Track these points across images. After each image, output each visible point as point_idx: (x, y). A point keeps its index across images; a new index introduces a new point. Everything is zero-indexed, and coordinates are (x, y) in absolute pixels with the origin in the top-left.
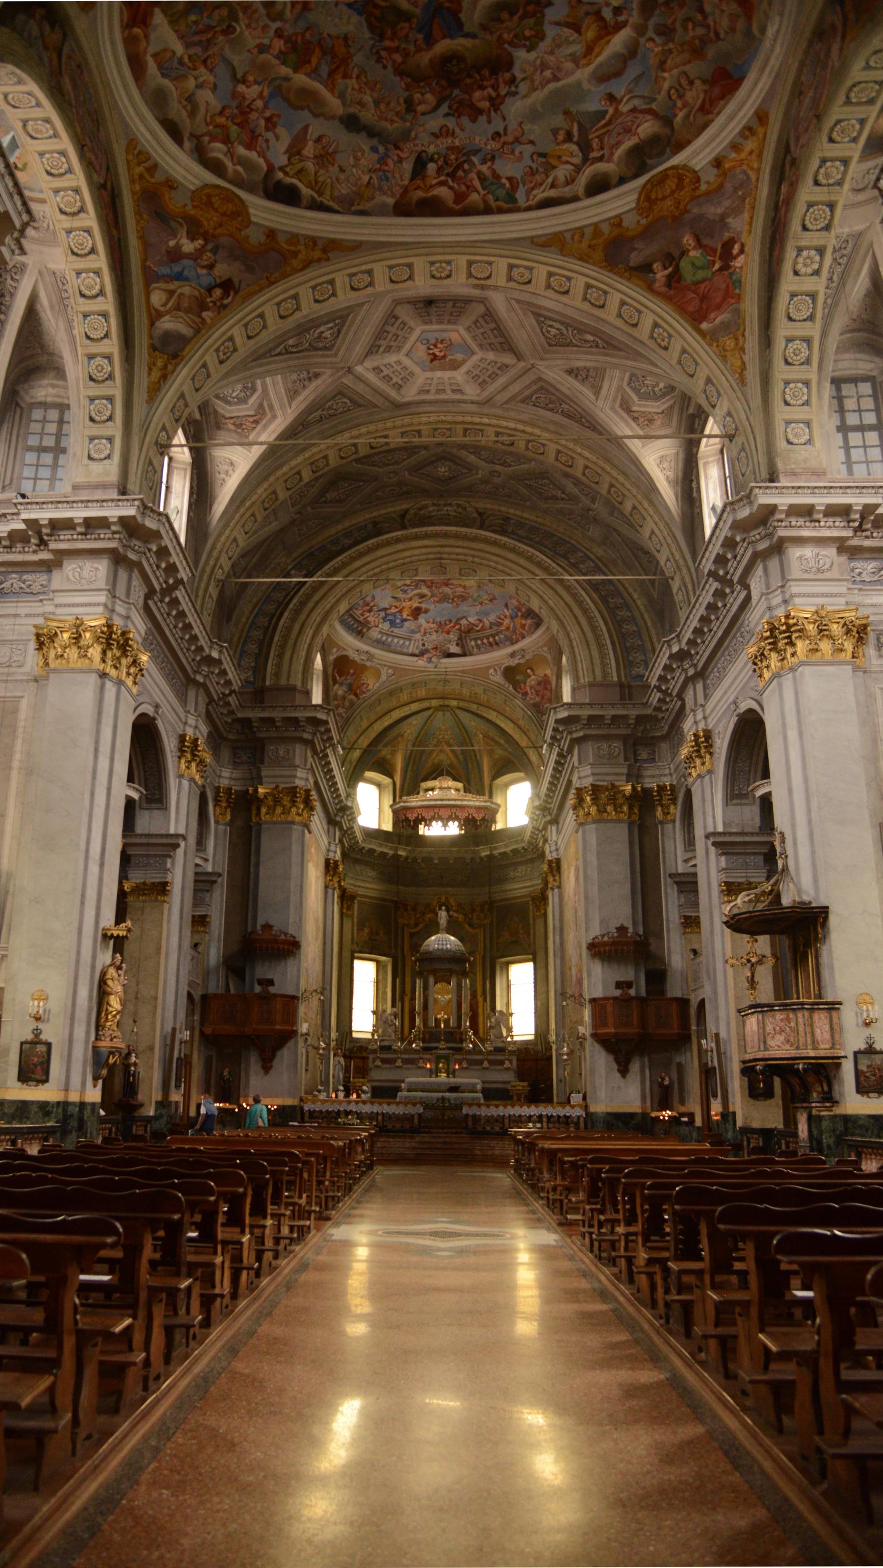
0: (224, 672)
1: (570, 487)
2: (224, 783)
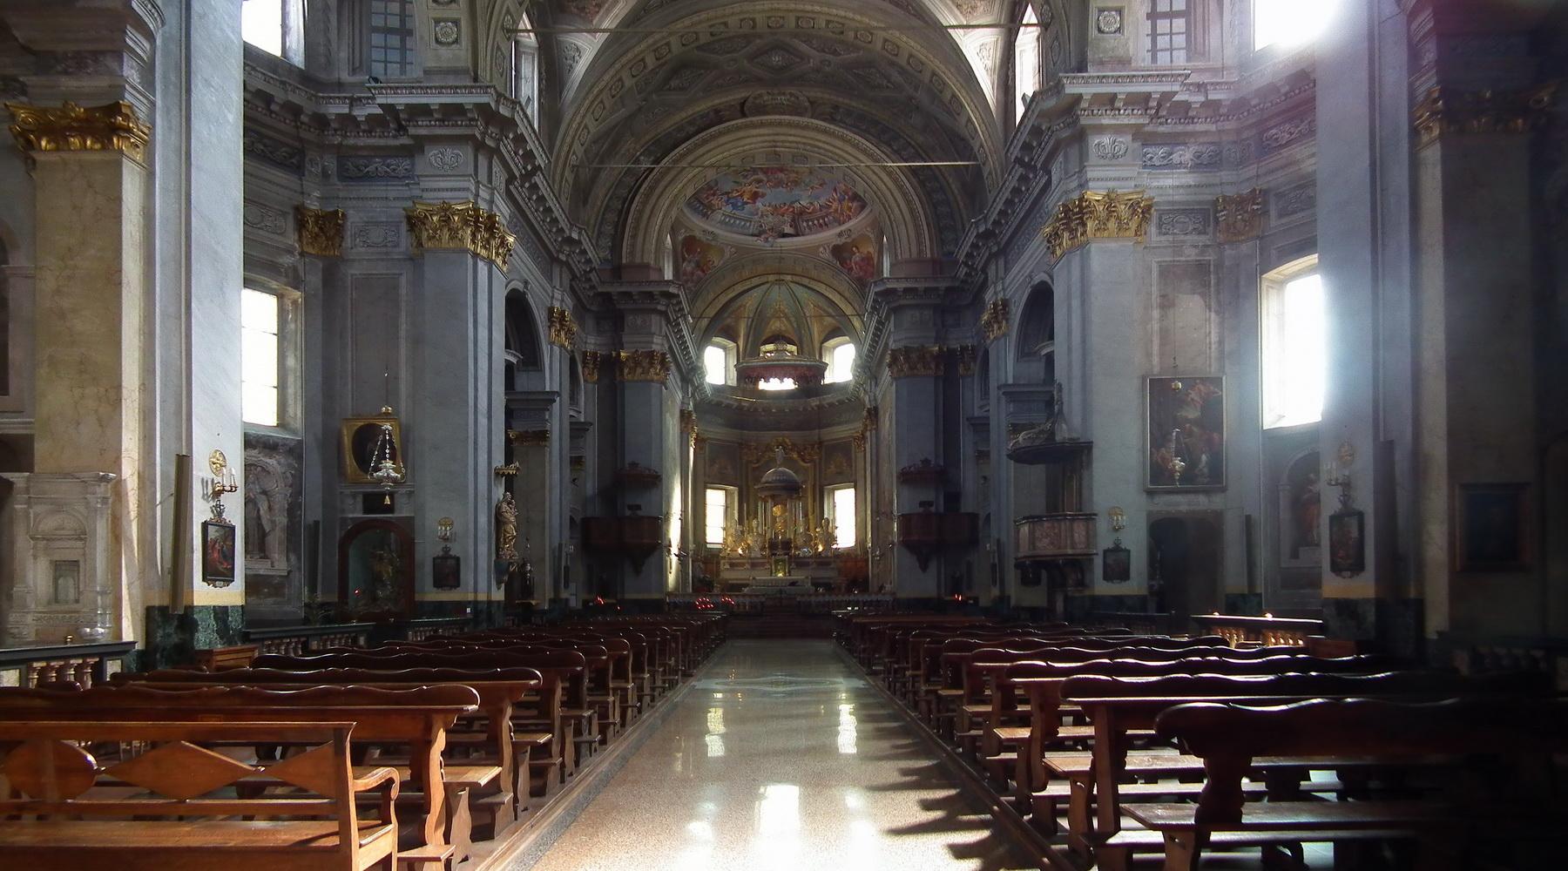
0: (584, 252)
1: (897, 78)
2: (590, 348)
